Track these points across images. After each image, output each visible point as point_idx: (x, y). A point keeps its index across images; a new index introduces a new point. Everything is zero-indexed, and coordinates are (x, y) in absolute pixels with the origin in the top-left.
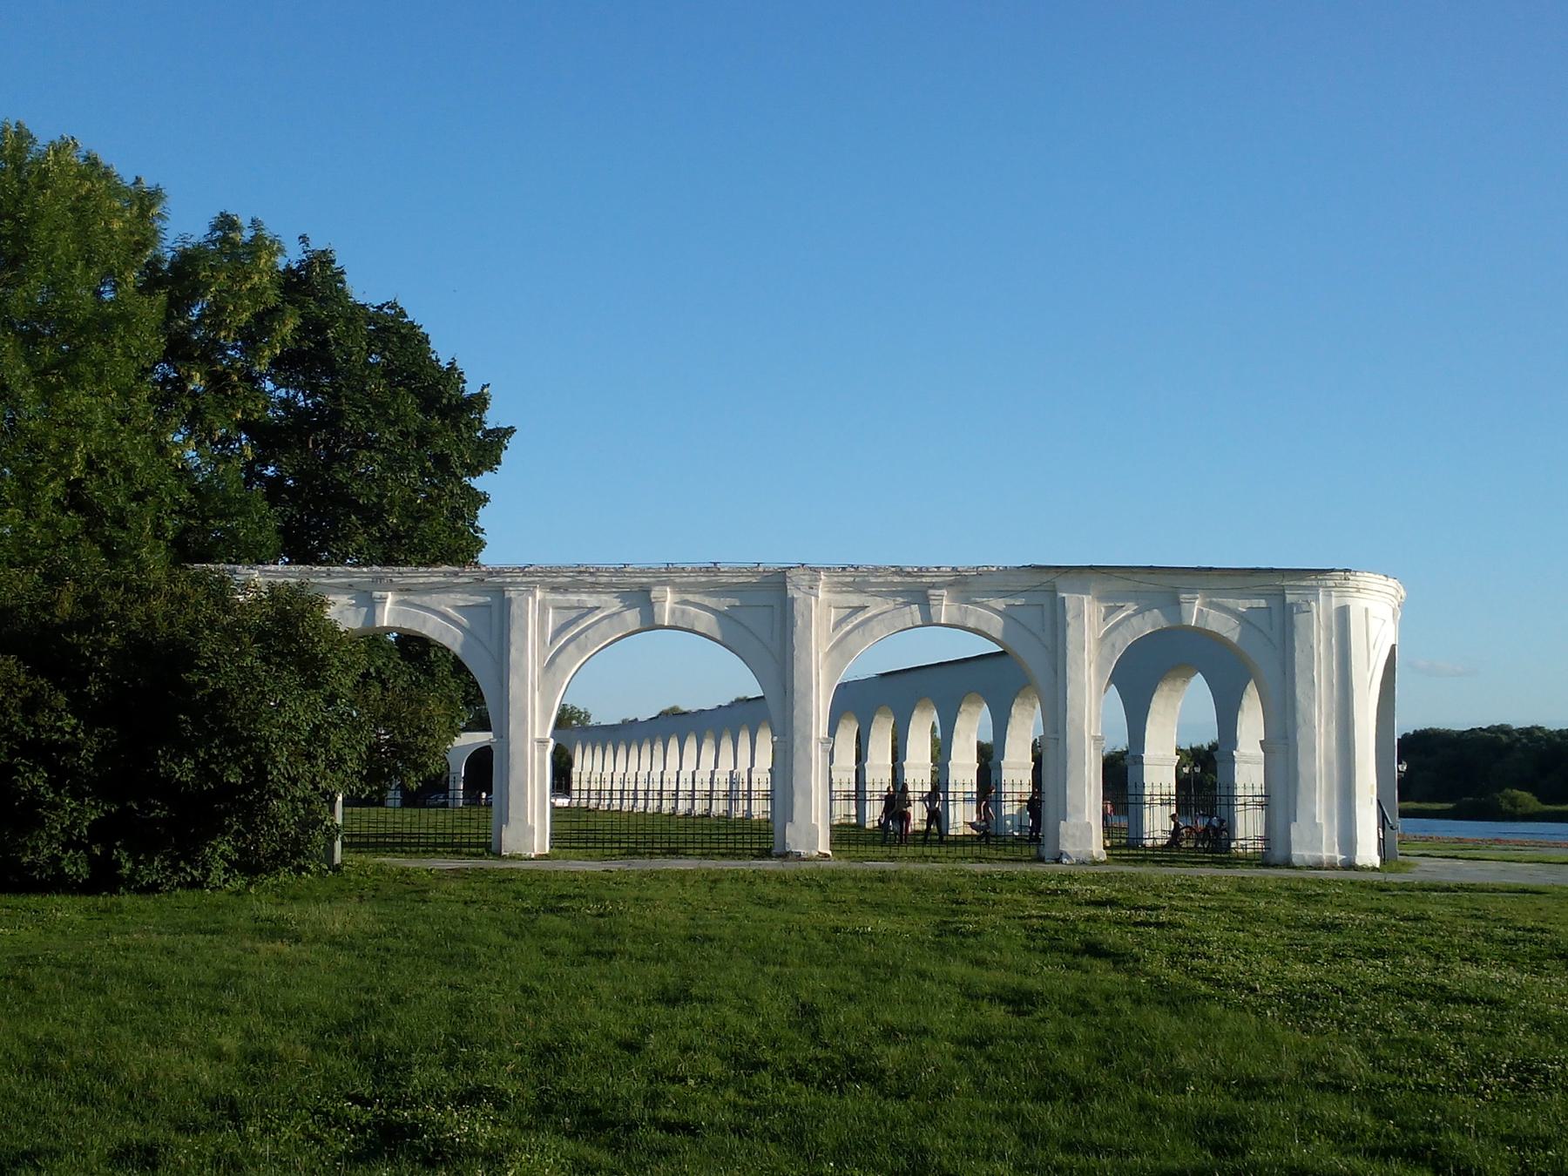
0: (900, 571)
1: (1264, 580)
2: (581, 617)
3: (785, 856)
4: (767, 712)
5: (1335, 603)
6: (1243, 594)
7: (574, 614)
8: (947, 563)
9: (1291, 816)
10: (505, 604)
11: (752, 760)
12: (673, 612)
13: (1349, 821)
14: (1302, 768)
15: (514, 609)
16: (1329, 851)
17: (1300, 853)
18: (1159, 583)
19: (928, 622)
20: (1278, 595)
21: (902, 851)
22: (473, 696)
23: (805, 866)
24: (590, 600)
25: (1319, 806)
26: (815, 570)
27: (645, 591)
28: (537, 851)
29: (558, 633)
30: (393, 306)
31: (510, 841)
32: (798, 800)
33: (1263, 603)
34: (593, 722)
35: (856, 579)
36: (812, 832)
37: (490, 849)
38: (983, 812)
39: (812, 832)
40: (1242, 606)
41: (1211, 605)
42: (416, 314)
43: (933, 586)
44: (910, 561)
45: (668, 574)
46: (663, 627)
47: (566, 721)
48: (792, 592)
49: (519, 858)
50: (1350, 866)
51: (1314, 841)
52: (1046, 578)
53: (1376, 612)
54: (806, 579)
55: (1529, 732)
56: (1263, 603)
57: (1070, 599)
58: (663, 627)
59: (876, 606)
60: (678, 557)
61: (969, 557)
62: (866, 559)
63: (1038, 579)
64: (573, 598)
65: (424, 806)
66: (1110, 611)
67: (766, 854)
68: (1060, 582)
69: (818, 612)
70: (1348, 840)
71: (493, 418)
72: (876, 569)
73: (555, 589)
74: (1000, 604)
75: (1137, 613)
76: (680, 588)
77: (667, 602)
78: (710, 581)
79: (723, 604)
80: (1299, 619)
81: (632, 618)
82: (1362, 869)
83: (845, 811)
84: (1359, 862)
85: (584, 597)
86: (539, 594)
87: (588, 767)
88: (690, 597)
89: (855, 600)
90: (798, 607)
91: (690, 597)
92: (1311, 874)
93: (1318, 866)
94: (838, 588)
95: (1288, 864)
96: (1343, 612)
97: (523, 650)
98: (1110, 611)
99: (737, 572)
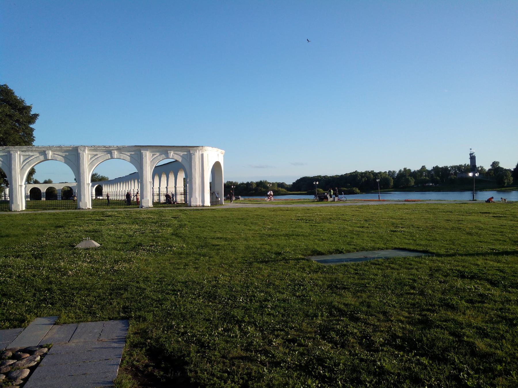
0: (105, 147)
1: (186, 148)
2: (29, 158)
3: (79, 209)
4: (137, 177)
5: (200, 153)
6: (181, 151)
7: (28, 157)
8: (115, 145)
9: (191, 196)
10: (10, 155)
11: (133, 188)
12: (51, 156)
13: (202, 198)
14: (193, 187)
15: (13, 156)
16: (199, 203)
17: (193, 204)
18: (164, 150)
19: (112, 158)
20: (188, 151)
21: (131, 206)
22: (4, 176)
23: (82, 211)
24: (31, 154)
25: (197, 194)
26: (85, 147)
27: (44, 152)
28: (20, 210)
29: (24, 161)
30: (5, 85)
31: (82, 205)
32: (82, 197)
33: (186, 153)
34: (109, 179)
35: (94, 149)
36: (148, 202)
37: (77, 207)
38: (185, 198)
39: (148, 202)
40: (182, 154)
41: (175, 154)
42: (11, 87)
43: (113, 150)
44: (107, 144)
45: (50, 148)
46: (49, 160)
47: (95, 179)
48: (79, 151)
49: (16, 211)
50: (203, 206)
51: (196, 201)
52: (138, 148)
53: (212, 155)
54: (83, 149)
55: (324, 177)
56: (186, 153)
57: (143, 152)
58: (49, 160)
59: (100, 154)
60: (51, 144)
61: (120, 144)
62: (97, 144)
63: (136, 148)
64: (27, 153)
65: (70, 199)
66: (153, 155)
67: (76, 209)
68: (167, 149)
69: (86, 156)
70: (203, 201)
71: (32, 112)
72: (99, 147)
73: (22, 151)
74: (129, 154)
75: (160, 155)
76: (52, 151)
77: (50, 154)
78: (60, 148)
79: (64, 155)
80: (193, 156)
81: (42, 158)
82: (206, 206)
83: (156, 198)
84: (205, 205)
85: (30, 153)
86: (19, 153)
87: (106, 189)
88: (55, 153)
89: (95, 153)
90: (81, 155)
91: (55, 153)
92: (195, 208)
93: (196, 206)
94: (90, 150)
95: (190, 206)
96: (202, 155)
97: (15, 165)
98: (153, 155)
99: (67, 147)
